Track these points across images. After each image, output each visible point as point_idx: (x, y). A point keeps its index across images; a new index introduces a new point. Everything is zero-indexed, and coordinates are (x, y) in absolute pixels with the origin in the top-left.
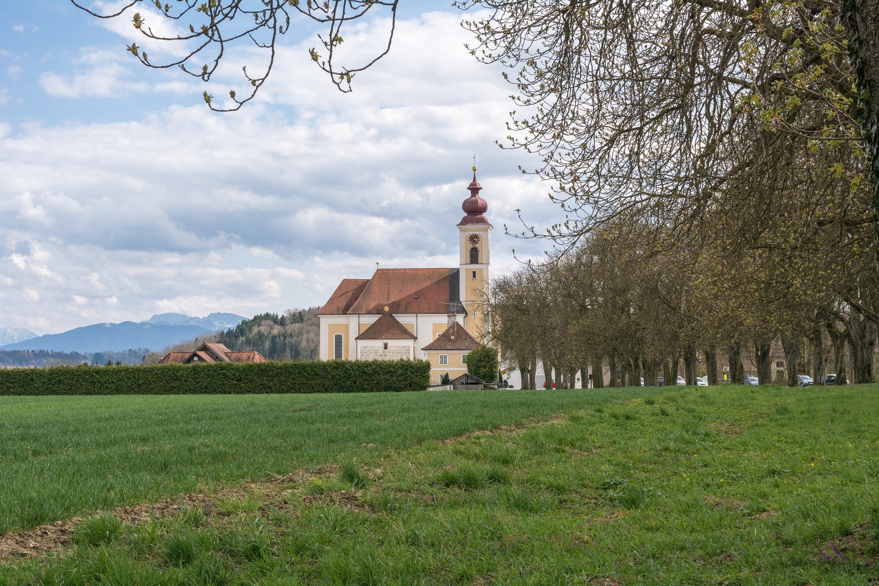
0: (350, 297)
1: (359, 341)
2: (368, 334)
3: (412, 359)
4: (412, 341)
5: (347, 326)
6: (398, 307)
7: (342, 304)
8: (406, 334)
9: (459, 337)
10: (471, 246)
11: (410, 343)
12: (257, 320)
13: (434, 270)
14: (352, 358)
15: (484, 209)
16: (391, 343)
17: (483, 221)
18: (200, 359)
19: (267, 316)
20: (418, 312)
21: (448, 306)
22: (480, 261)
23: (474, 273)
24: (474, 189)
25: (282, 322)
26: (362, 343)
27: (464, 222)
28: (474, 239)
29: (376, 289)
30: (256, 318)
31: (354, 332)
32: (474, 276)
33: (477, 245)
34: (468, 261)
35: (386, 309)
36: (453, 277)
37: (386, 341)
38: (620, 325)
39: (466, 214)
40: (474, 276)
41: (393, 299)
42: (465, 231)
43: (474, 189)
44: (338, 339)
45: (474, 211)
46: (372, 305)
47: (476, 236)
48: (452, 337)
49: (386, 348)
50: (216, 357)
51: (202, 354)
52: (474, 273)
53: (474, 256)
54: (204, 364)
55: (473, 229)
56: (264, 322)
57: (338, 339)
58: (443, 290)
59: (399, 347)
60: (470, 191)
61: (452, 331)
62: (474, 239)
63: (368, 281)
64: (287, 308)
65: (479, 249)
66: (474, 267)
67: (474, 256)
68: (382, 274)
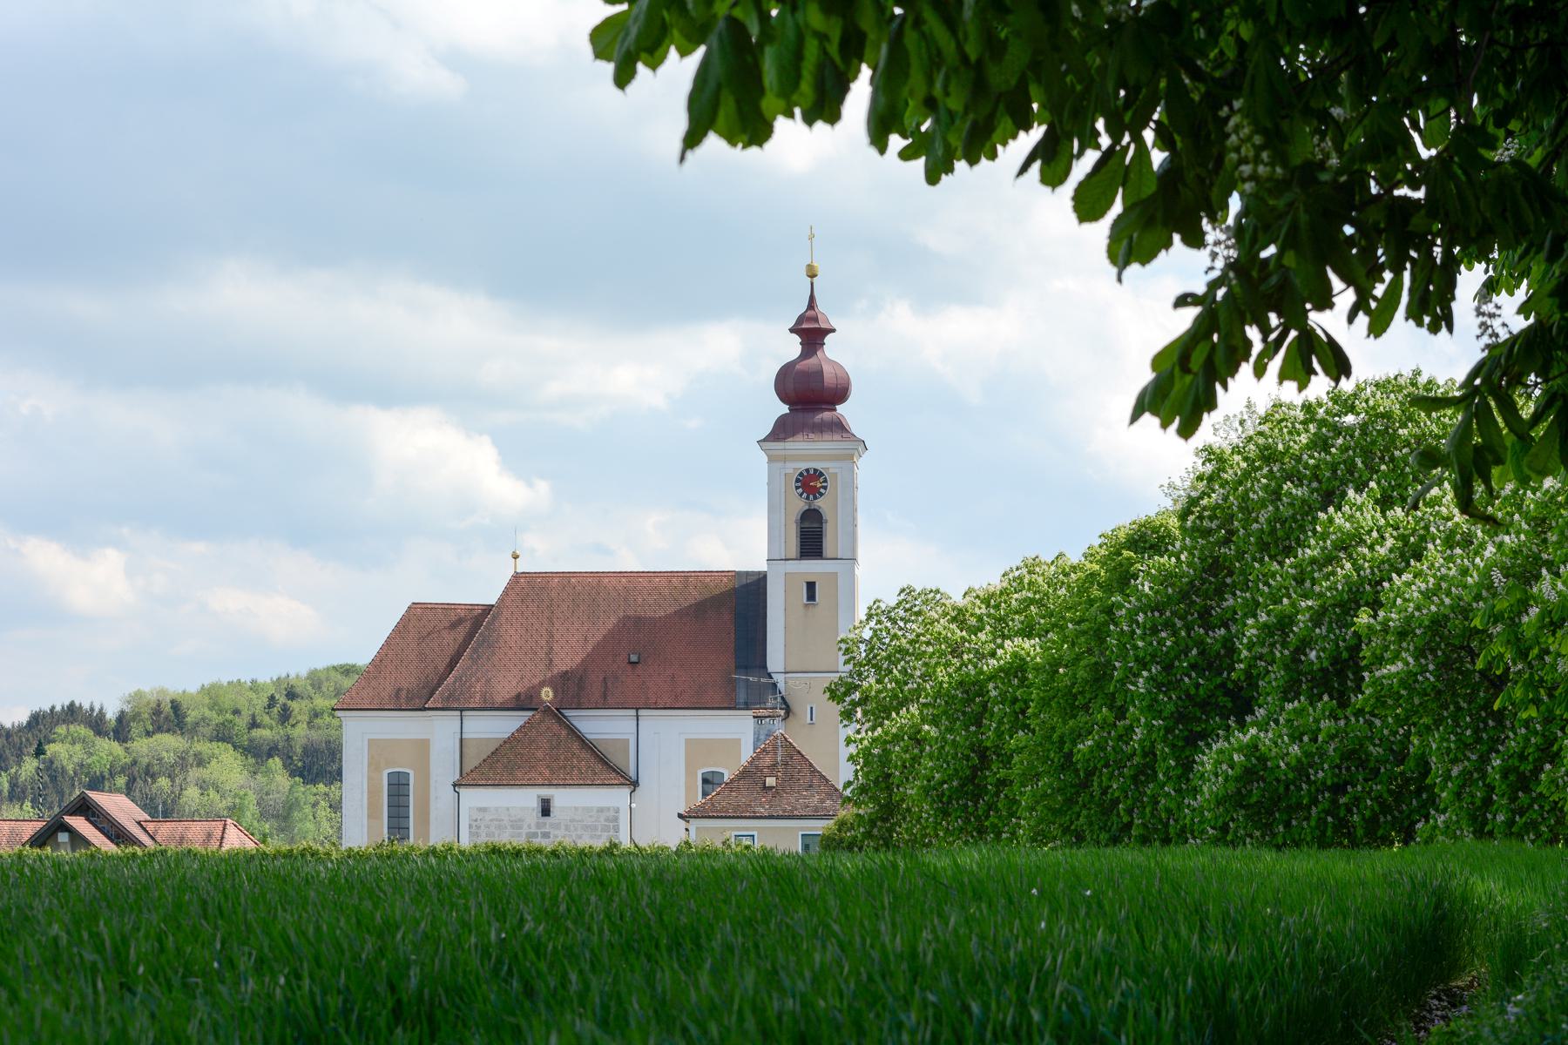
0: (438, 655)
1: (462, 791)
2: (492, 768)
3: (626, 843)
4: (626, 791)
5: (423, 747)
6: (578, 688)
7: (409, 679)
8: (607, 768)
9: (788, 781)
10: (800, 505)
11: (616, 797)
12: (41, 725)
13: (685, 576)
14: (438, 836)
15: (840, 393)
16: (563, 798)
17: (839, 427)
18: (77, 839)
19: (72, 713)
20: (639, 703)
21: (732, 684)
22: (828, 547)
23: (811, 586)
24: (812, 333)
25: (121, 730)
26: (474, 798)
27: (782, 431)
28: (810, 483)
29: (510, 633)
30: (36, 719)
31: (444, 768)
32: (811, 596)
33: (821, 503)
34: (794, 549)
35: (547, 694)
36: (743, 600)
37: (546, 792)
38: (1382, 551)
39: (785, 409)
40: (811, 596)
41: (566, 661)
42: (785, 459)
43: (812, 333)
44: (398, 786)
45: (810, 397)
46: (507, 687)
47: (818, 474)
48: (771, 781)
49: (546, 810)
50: (117, 834)
51: (79, 823)
52: (811, 586)
53: (811, 538)
54: (81, 852)
55: (808, 450)
56: (61, 730)
57: (398, 786)
58: (711, 636)
59: (587, 810)
60: (796, 339)
61: (768, 761)
62: (810, 483)
63: (488, 609)
64: (133, 689)
65: (794, 493)
66: (812, 567)
67: (811, 538)
68: (526, 587)
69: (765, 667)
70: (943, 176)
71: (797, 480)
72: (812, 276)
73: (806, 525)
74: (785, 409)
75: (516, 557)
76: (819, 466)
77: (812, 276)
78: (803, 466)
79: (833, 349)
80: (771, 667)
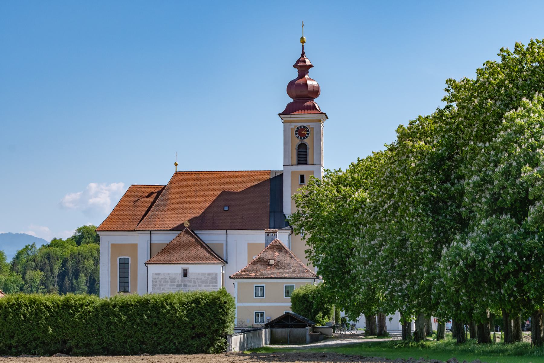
10: (298, 142)
23: (302, 177)
28: (302, 132)
33: (306, 141)
52: (302, 177)
55: (301, 118)
65: (295, 137)
66: (302, 168)
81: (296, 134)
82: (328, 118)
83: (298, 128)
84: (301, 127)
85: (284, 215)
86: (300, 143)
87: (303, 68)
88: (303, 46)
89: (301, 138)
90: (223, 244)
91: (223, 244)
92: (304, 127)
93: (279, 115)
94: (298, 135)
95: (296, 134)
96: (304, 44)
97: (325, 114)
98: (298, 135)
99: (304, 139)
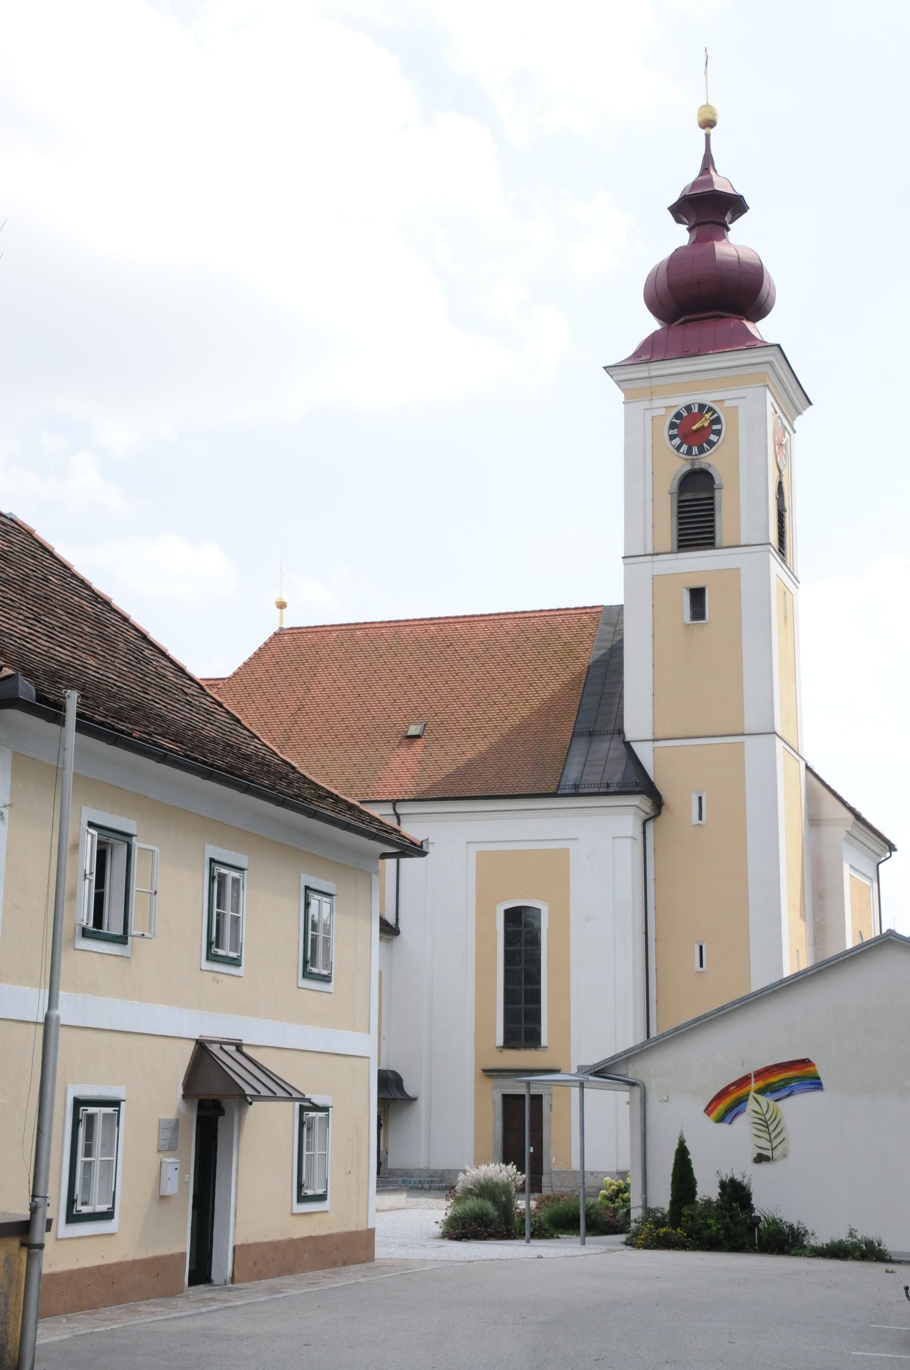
10: (679, 465)
23: (697, 595)
28: (694, 429)
33: (711, 460)
42: (652, 394)
52: (697, 595)
55: (699, 379)
62: (694, 429)
65: (669, 446)
66: (697, 563)
69: (621, 732)
70: (689, 1157)
71: (672, 426)
72: (708, 124)
73: (688, 496)
74: (652, 325)
75: (282, 605)
76: (707, 398)
77: (708, 124)
78: (680, 401)
79: (741, 239)
80: (632, 731)
81: (672, 437)
82: (811, 404)
83: (678, 415)
84: (688, 408)
85: (627, 745)
86: (688, 467)
87: (708, 207)
88: (708, 137)
89: (689, 452)
90: (479, 854)
91: (479, 854)
92: (702, 407)
93: (605, 368)
94: (677, 441)
95: (672, 437)
96: (713, 132)
97: (779, 346)
98: (677, 441)
99: (702, 451)
